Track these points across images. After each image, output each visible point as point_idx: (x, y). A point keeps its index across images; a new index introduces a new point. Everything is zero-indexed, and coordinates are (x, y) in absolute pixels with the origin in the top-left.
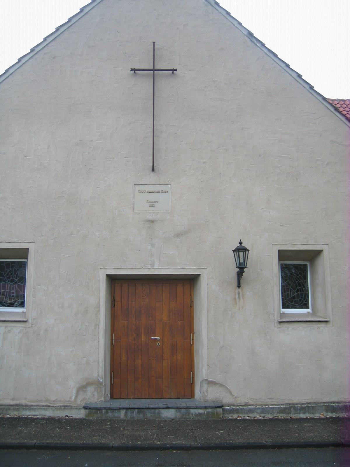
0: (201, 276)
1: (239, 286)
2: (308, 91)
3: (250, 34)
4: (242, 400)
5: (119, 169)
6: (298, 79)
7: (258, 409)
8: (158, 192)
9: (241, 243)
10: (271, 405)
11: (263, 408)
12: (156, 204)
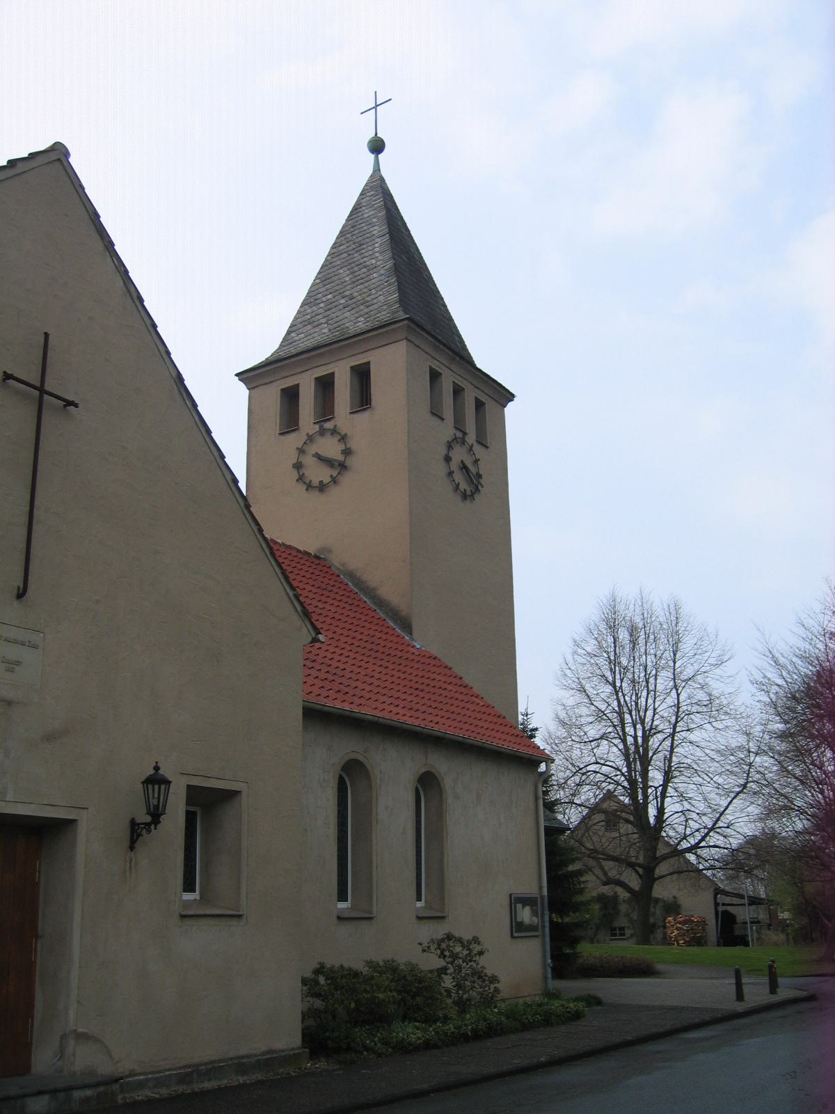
0: (79, 823)
1: (132, 848)
2: (242, 510)
3: (180, 379)
4: (125, 1066)
5: (716, 805)
6: (232, 484)
7: (150, 1079)
8: (23, 644)
9: (157, 768)
10: (169, 1070)
11: (157, 1078)
12: (17, 668)
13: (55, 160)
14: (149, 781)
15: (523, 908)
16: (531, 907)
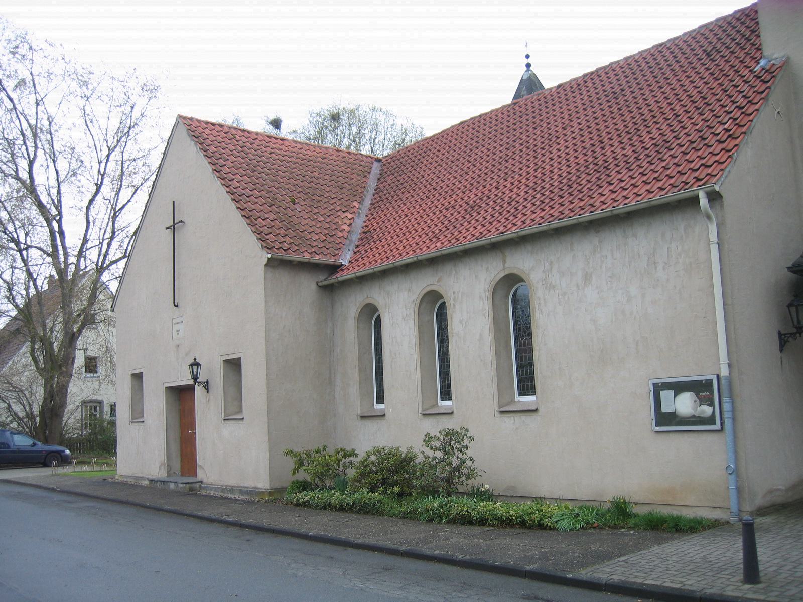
9: (195, 359)
13: (37, 109)
14: (192, 365)
15: (675, 396)
16: (697, 395)
